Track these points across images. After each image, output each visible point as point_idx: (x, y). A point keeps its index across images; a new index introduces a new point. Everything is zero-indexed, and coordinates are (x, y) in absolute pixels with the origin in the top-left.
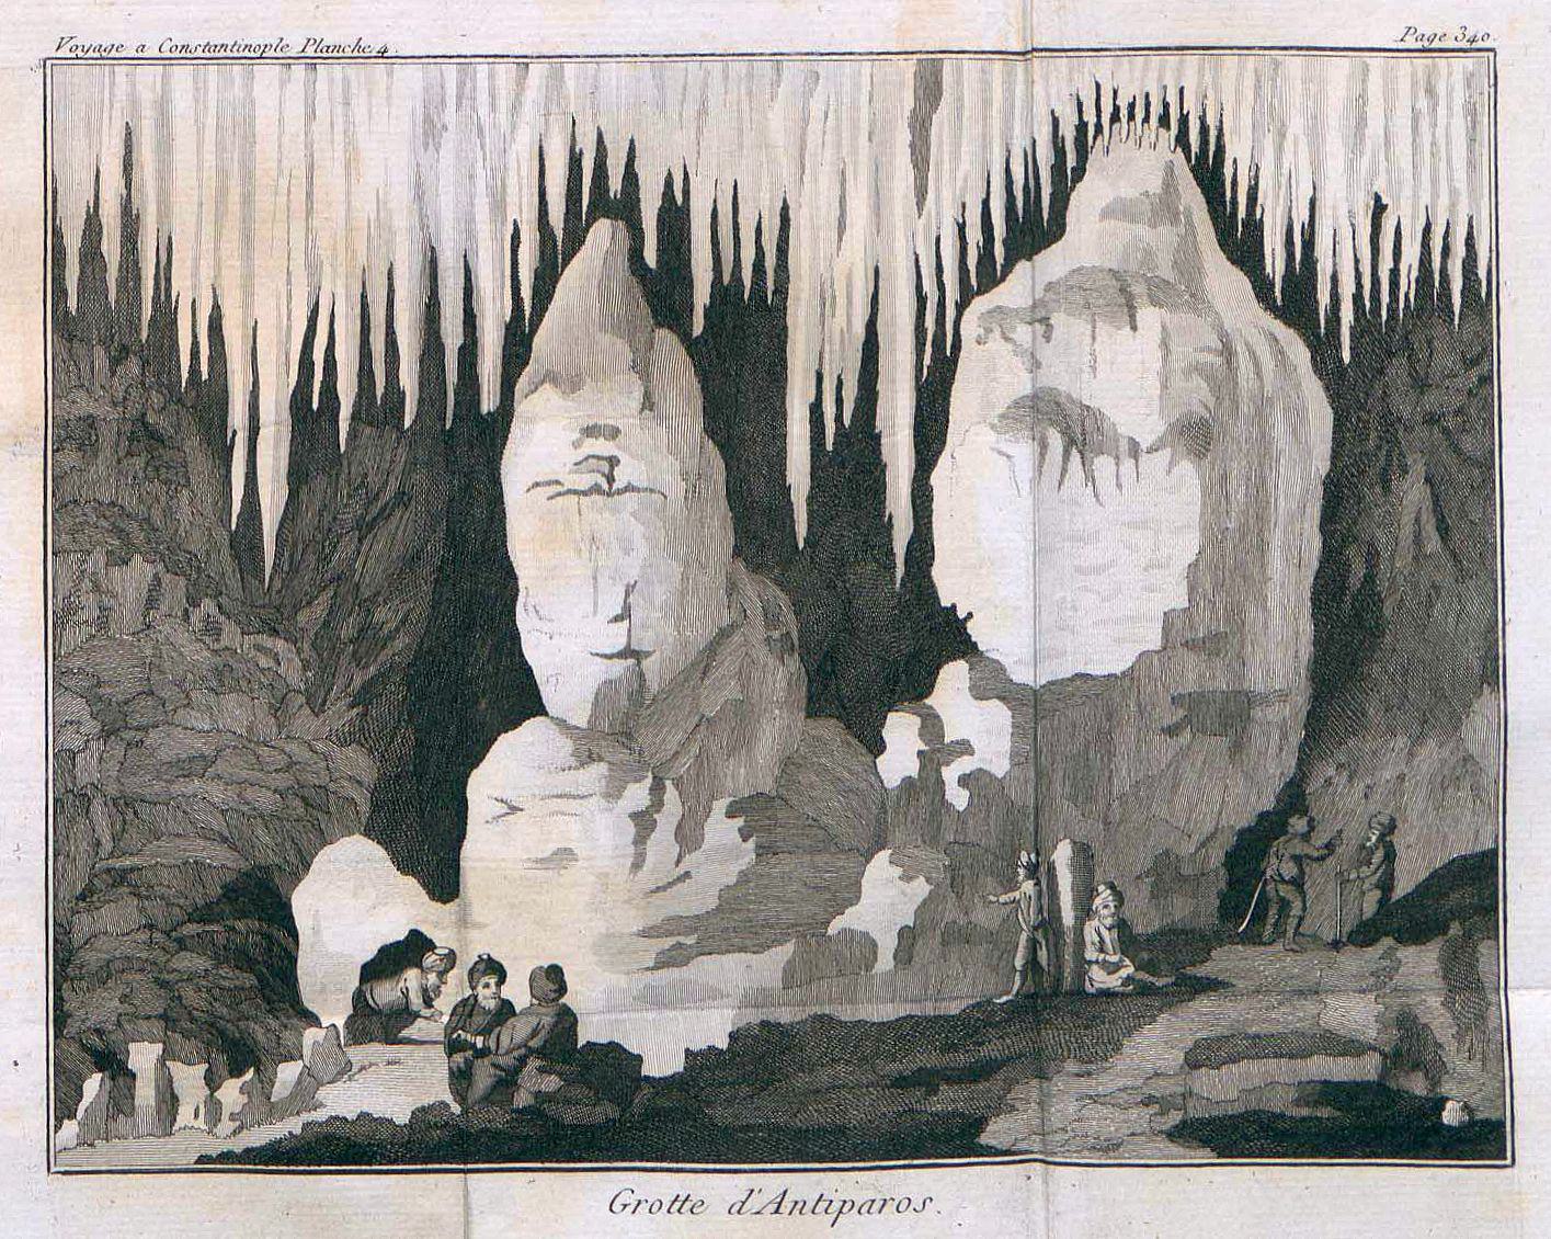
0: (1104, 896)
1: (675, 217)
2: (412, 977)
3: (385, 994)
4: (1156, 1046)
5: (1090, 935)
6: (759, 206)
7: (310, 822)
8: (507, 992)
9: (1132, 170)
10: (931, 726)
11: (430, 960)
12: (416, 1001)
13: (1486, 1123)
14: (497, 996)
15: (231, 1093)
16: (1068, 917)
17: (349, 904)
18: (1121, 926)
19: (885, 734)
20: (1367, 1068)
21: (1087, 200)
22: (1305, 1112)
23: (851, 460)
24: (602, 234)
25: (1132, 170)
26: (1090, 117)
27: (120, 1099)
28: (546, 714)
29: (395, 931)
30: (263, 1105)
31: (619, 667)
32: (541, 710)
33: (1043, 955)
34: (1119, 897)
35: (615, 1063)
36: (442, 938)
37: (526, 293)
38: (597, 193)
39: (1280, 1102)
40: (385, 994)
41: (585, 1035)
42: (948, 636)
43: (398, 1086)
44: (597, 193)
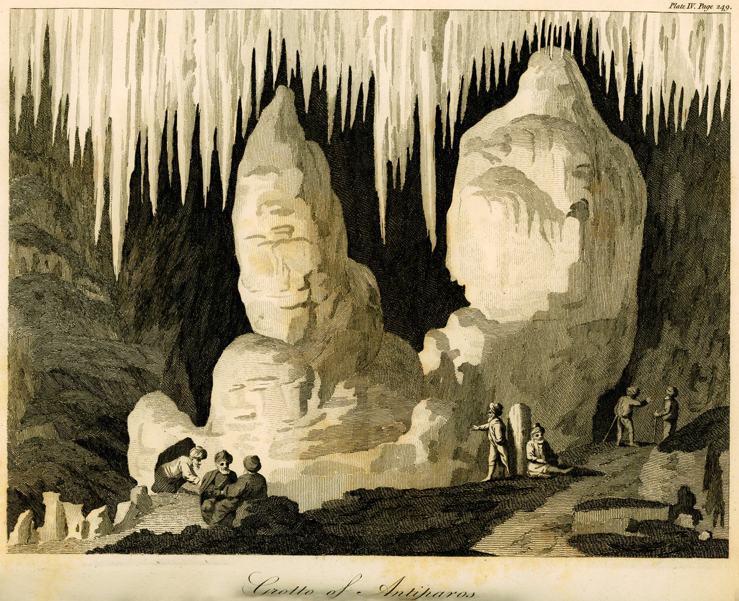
0: (536, 430)
1: (319, 91)
2: (183, 459)
3: (172, 468)
4: (559, 506)
5: (529, 449)
6: (361, 79)
7: (143, 383)
8: (232, 467)
9: (544, 86)
10: (443, 343)
11: (193, 453)
12: (186, 473)
13: (718, 541)
14: (227, 469)
15: (95, 517)
16: (518, 443)
17: (152, 427)
18: (546, 446)
19: (44, 502)
20: (662, 514)
21: (527, 79)
22: (628, 534)
23: (406, 194)
24: (282, 95)
25: (544, 86)
26: (531, 39)
27: (38, 519)
28: (252, 332)
29: (182, 437)
30: (109, 524)
31: (299, 311)
32: (246, 328)
33: (504, 459)
34: (542, 430)
35: (286, 506)
36: (198, 440)
37: (244, 126)
38: (278, 77)
39: (620, 529)
40: (172, 468)
41: (270, 493)
42: (454, 297)
43: (176, 516)
44: (278, 77)
